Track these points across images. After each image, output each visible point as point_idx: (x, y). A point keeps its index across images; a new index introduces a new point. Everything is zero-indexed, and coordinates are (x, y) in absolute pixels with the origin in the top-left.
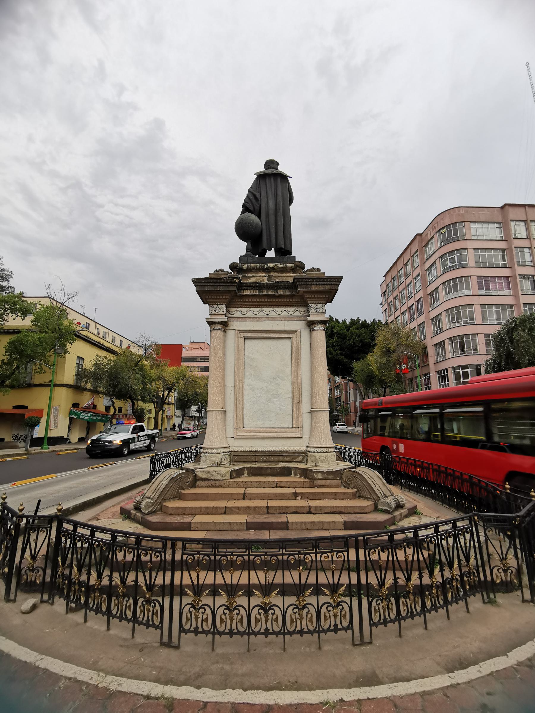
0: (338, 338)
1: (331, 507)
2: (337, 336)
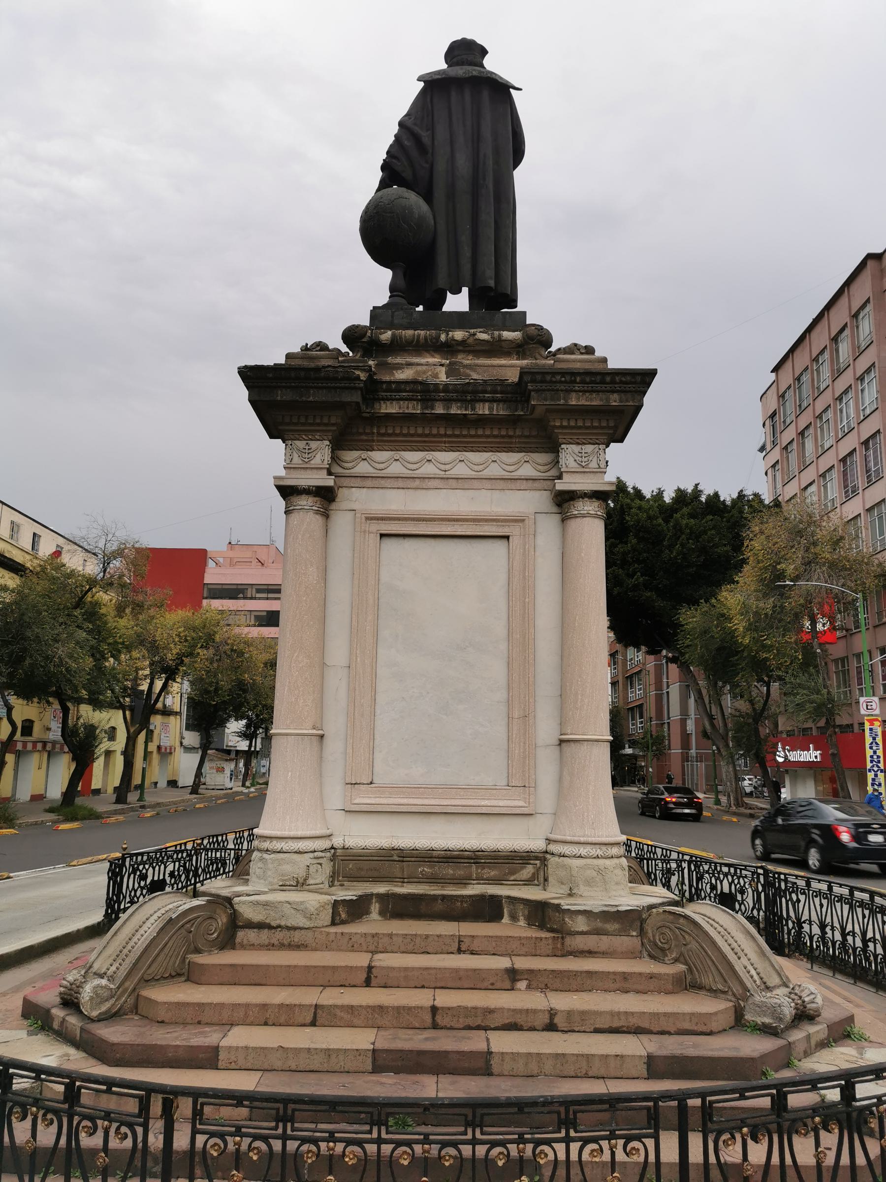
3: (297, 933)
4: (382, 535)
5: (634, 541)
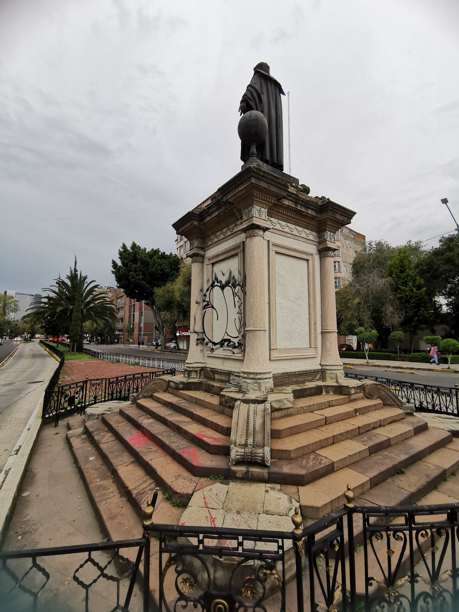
0: (142, 264)
1: (390, 417)
2: (140, 262)
3: (289, 410)
4: (276, 252)
5: (140, 264)
